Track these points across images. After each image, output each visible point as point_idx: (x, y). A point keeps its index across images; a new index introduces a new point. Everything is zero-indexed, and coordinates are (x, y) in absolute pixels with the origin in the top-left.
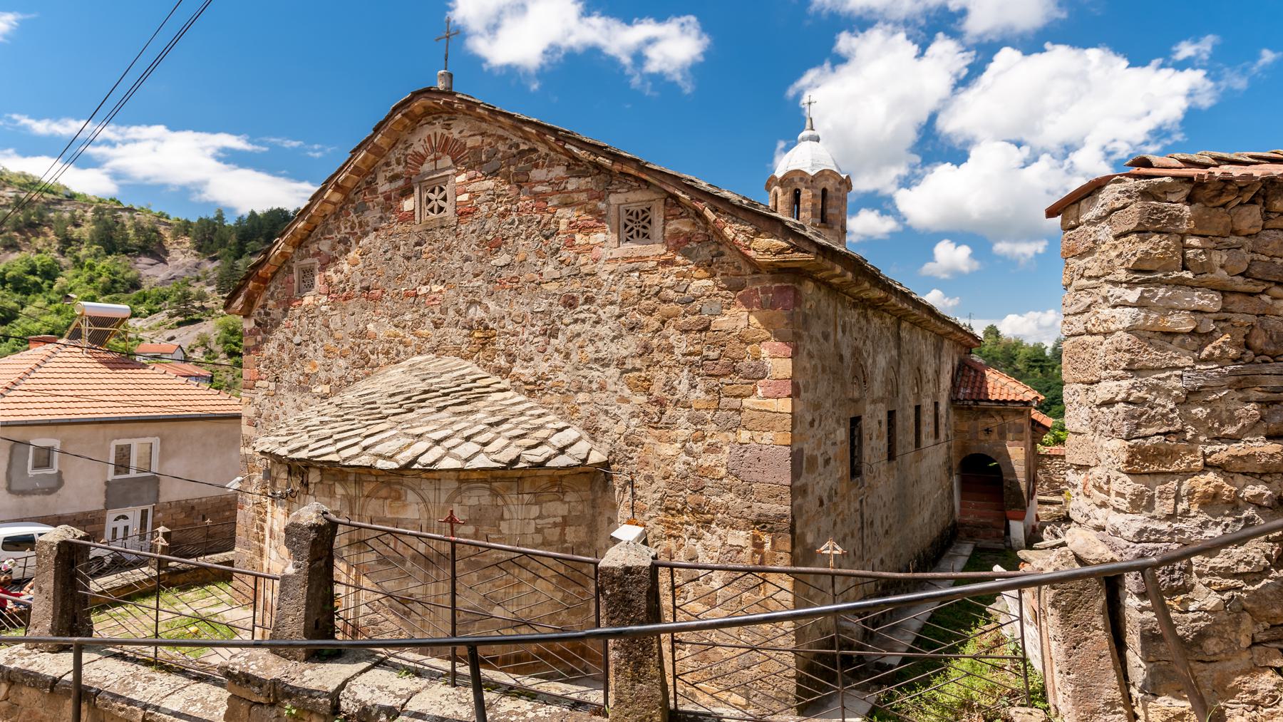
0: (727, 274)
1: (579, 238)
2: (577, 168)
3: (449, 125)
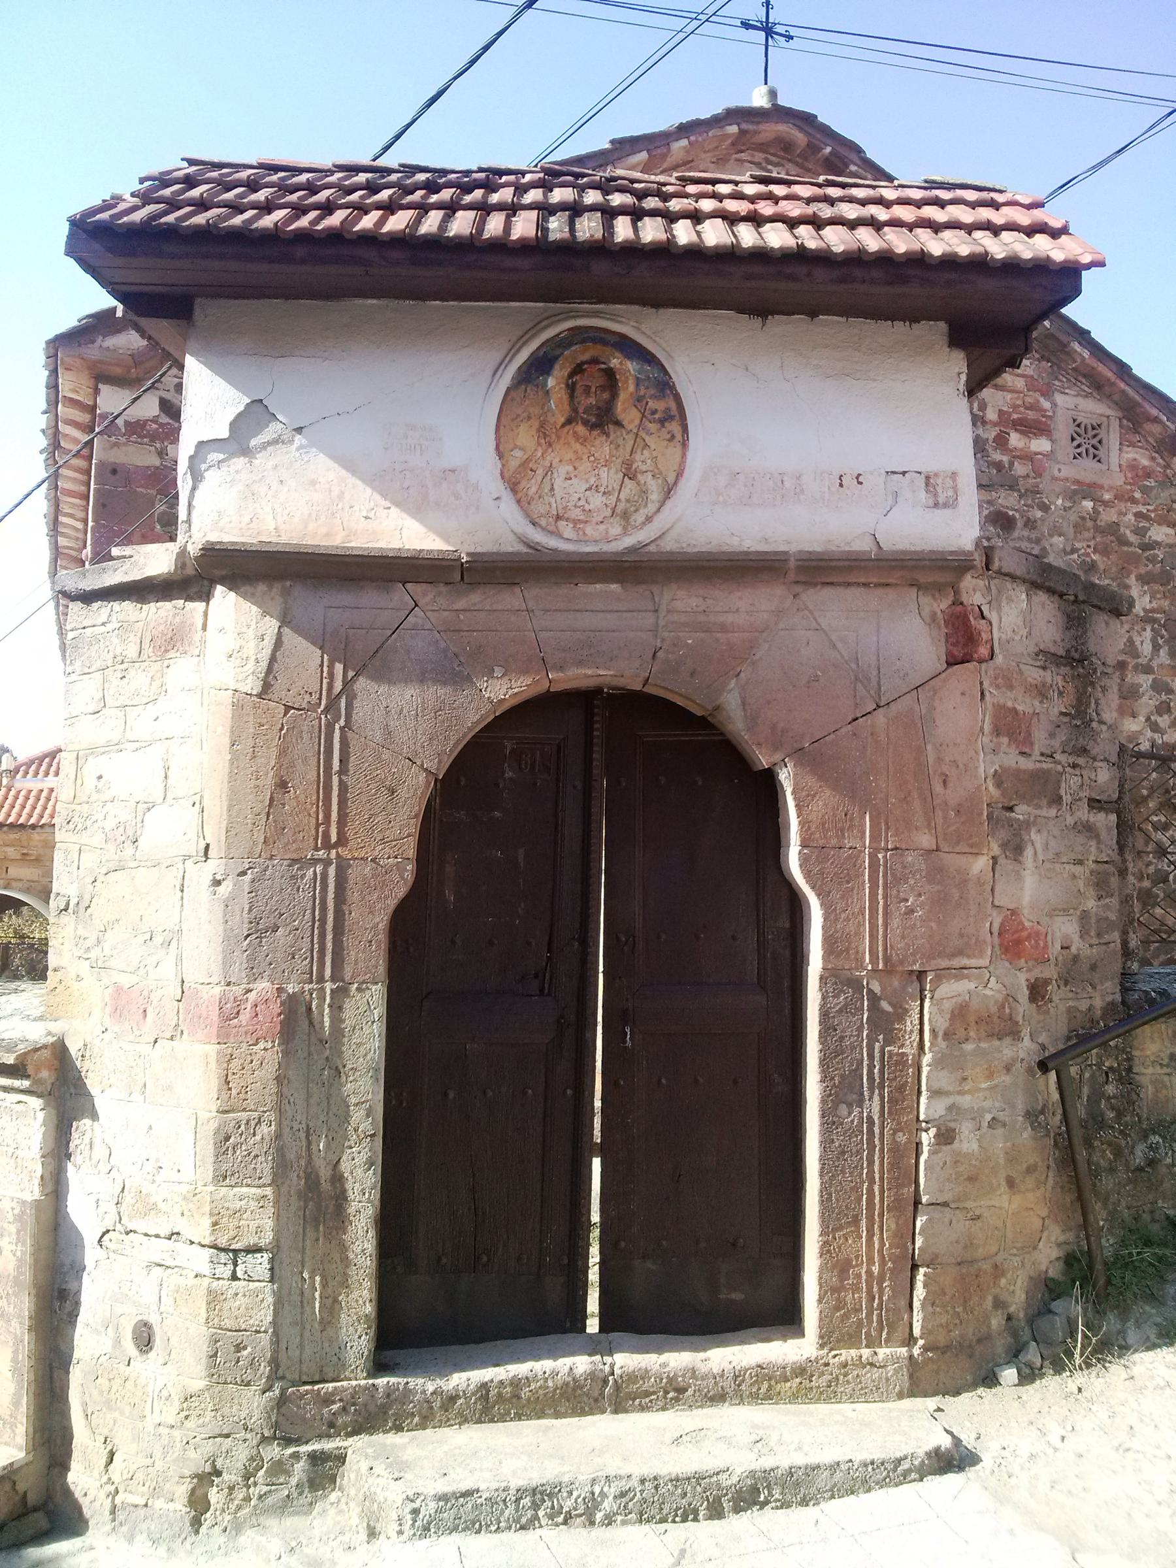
1: (1015, 440)
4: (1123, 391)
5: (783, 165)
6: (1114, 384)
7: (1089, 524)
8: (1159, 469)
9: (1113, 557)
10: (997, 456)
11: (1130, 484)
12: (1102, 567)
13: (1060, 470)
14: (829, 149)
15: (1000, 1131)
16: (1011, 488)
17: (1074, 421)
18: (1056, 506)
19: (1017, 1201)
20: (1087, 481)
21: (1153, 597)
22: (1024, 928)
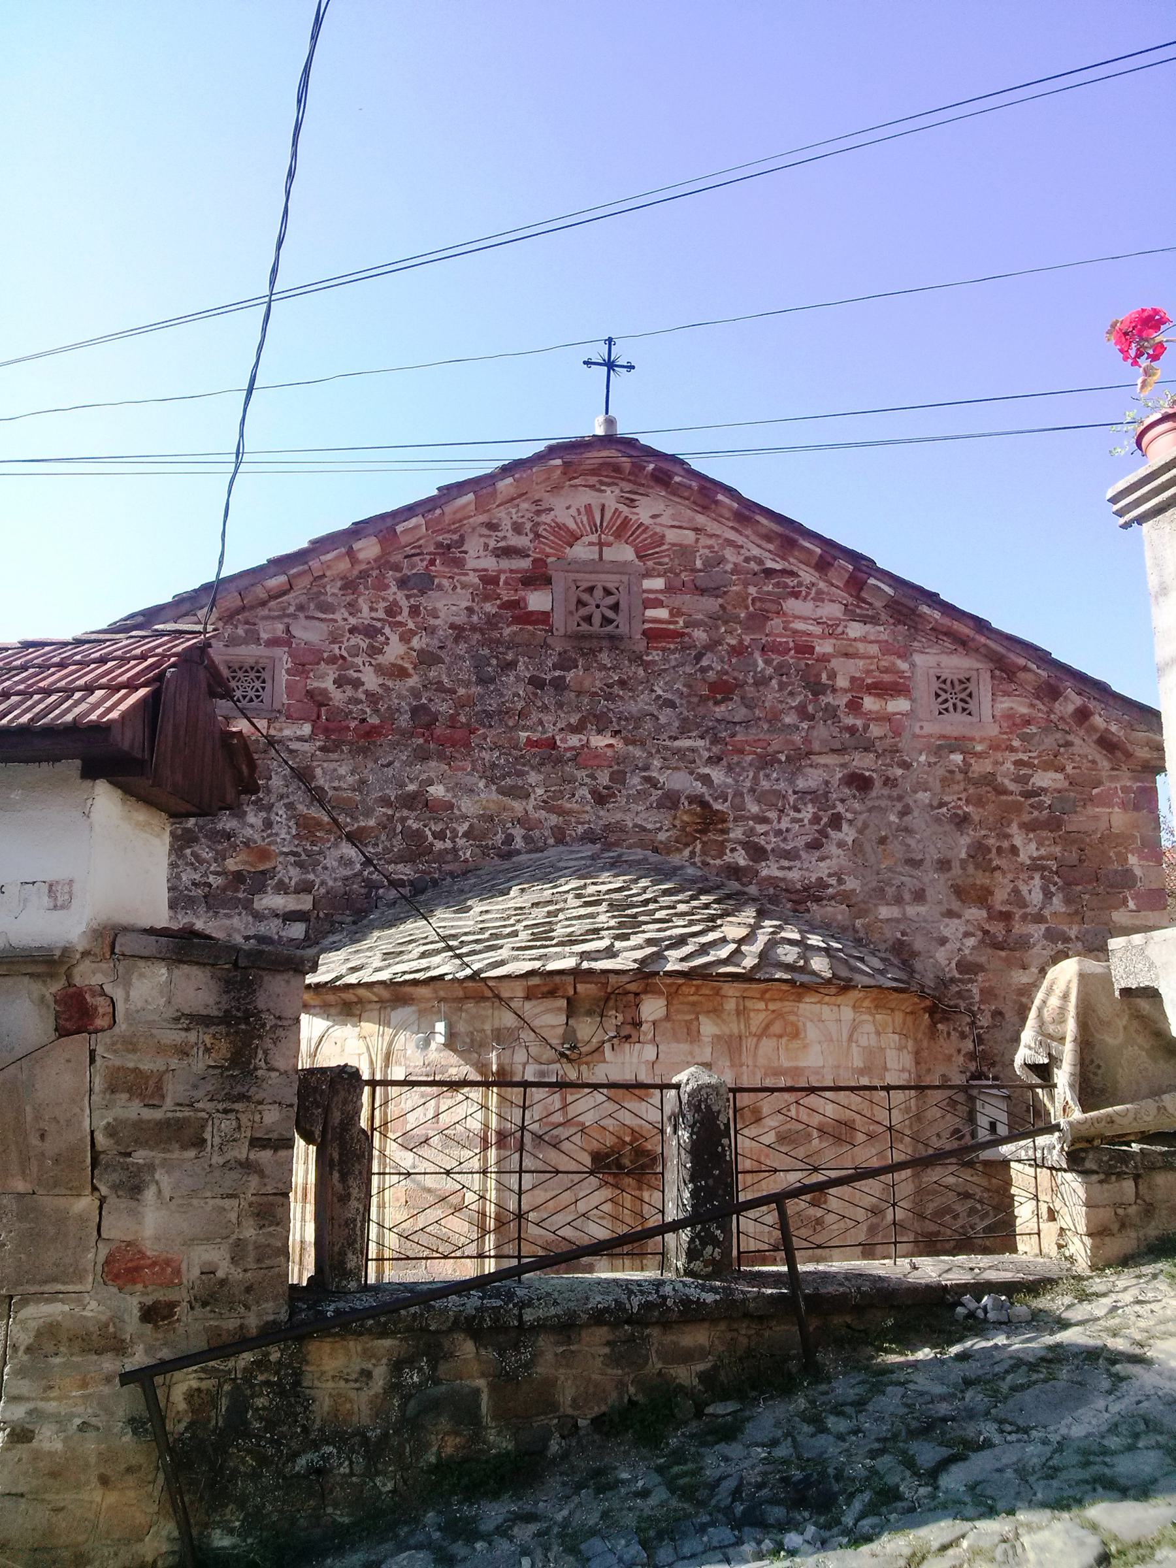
0: (1079, 768)
1: (870, 703)
2: (858, 611)
3: (633, 500)
4: (985, 645)
5: (617, 484)
6: (973, 639)
7: (959, 777)
8: (1040, 715)
9: (991, 807)
10: (850, 721)
11: (1005, 733)
12: (976, 818)
13: (921, 728)
14: (652, 466)
15: (91, 1434)
16: (866, 750)
17: (938, 678)
18: (919, 763)
19: (112, 1498)
20: (955, 734)
21: (1040, 844)
22: (143, 1256)
